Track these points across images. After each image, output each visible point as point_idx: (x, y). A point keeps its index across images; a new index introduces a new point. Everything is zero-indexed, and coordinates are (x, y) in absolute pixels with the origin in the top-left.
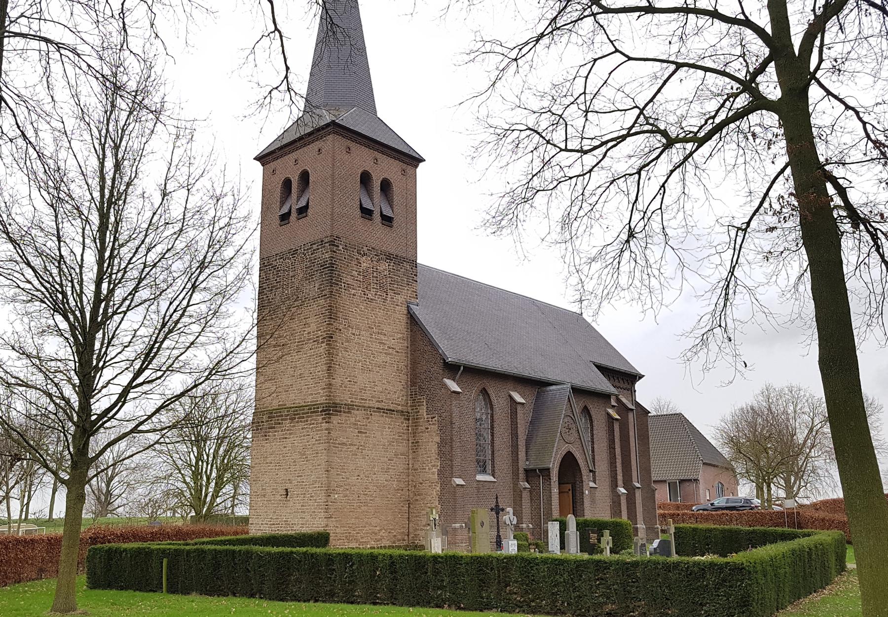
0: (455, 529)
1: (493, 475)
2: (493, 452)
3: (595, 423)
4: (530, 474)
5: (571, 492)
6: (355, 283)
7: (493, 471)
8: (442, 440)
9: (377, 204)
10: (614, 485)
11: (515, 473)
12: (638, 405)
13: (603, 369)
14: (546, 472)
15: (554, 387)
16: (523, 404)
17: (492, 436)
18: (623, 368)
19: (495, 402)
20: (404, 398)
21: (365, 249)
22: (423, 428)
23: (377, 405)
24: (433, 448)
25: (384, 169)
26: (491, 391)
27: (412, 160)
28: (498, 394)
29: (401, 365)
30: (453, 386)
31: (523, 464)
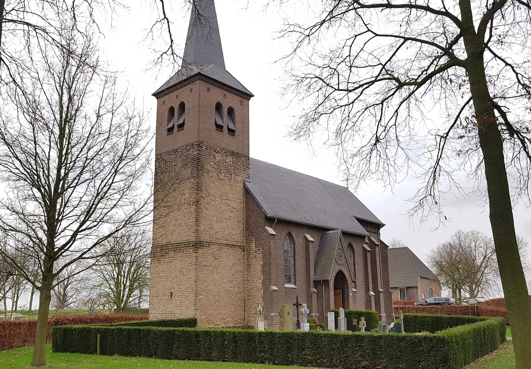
0: (272, 316)
1: (295, 284)
2: (295, 270)
3: (356, 253)
4: (317, 283)
5: (341, 294)
6: (212, 169)
7: (295, 282)
8: (264, 263)
9: (226, 122)
10: (367, 290)
11: (308, 283)
12: (381, 242)
13: (360, 221)
14: (326, 282)
15: (331, 232)
16: (313, 242)
17: (294, 261)
18: (372, 220)
19: (296, 240)
20: (242, 238)
21: (218, 149)
22: (253, 256)
23: (225, 242)
24: (259, 268)
25: (230, 101)
26: (293, 234)
27: (246, 96)
28: (298, 236)
29: (240, 218)
30: (271, 231)
31: (313, 277)
